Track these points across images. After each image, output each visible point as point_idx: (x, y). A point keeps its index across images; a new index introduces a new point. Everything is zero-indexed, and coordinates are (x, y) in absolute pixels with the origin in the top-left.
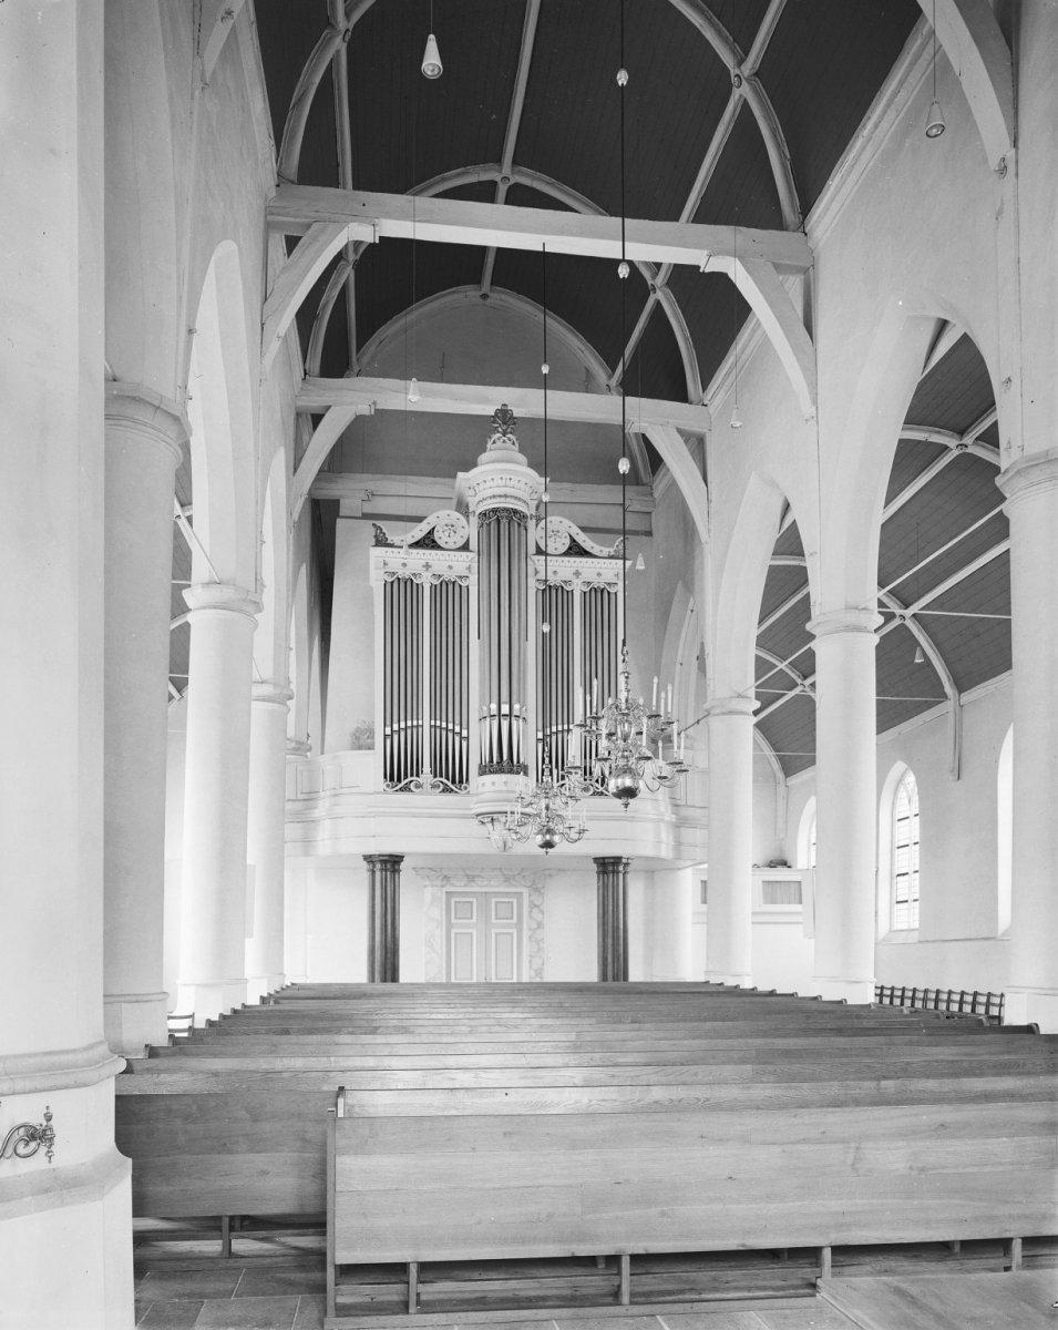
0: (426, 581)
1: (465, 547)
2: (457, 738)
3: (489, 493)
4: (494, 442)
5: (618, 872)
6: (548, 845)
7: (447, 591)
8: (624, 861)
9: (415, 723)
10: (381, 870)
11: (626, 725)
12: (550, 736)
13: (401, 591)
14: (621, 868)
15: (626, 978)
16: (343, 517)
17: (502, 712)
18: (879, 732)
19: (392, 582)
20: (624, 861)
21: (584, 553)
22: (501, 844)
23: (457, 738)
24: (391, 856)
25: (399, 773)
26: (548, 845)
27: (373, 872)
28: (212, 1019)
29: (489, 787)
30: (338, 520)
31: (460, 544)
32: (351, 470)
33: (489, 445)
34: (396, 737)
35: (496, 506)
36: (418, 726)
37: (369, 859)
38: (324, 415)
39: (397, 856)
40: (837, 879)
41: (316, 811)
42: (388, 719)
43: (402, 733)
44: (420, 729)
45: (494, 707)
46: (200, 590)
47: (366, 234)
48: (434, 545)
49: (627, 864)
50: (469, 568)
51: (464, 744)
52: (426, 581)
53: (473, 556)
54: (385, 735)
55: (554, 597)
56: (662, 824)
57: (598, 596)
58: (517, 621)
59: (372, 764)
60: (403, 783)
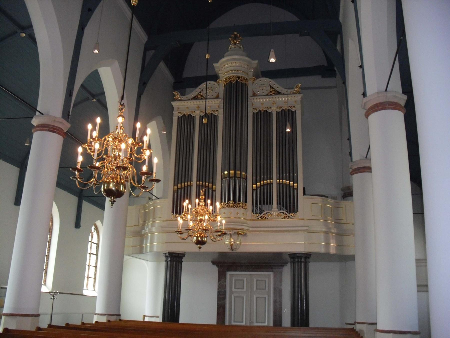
0: (274, 110)
1: (217, 97)
2: (210, 191)
5: (301, 262)
19: (257, 113)
21: (278, 93)
22: (229, 247)
28: (10, 328)
31: (215, 95)
33: (229, 49)
43: (183, 190)
50: (219, 106)
52: (197, 114)
55: (263, 117)
57: (287, 116)
58: (240, 130)
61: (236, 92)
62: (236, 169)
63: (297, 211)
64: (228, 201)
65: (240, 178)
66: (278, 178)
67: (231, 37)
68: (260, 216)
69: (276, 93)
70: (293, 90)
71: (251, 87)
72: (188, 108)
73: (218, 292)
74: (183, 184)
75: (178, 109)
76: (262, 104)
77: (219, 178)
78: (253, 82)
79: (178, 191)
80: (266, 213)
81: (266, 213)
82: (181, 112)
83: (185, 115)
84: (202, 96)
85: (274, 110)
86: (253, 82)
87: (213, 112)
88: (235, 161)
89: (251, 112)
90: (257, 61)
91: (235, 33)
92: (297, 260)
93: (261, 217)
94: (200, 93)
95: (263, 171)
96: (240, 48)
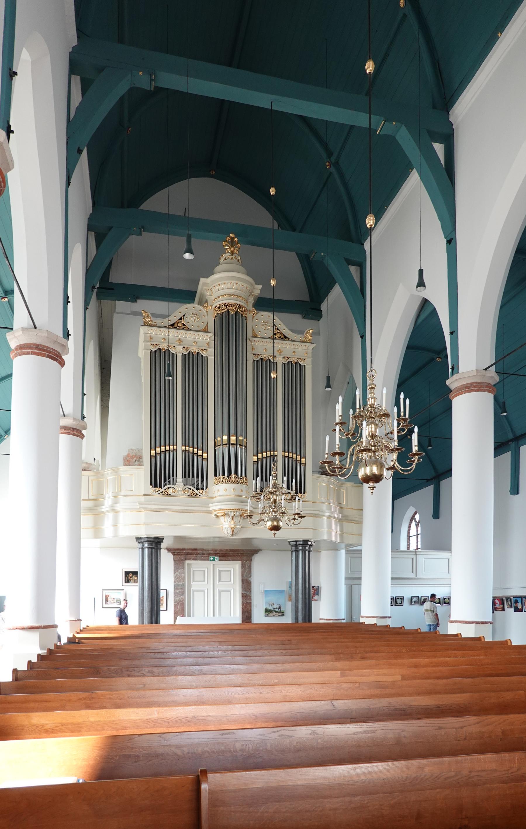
0: (179, 351)
1: (205, 330)
2: (200, 459)
3: (222, 292)
4: (225, 259)
6: (276, 528)
7: (194, 361)
8: (310, 543)
9: (167, 448)
10: (148, 548)
11: (373, 426)
12: (262, 459)
13: (161, 359)
14: (307, 548)
15: (310, 621)
16: (118, 313)
17: (232, 442)
18: (494, 457)
19: (155, 351)
20: (310, 543)
21: (285, 338)
22: (230, 531)
23: (200, 459)
24: (155, 538)
25: (160, 478)
26: (276, 528)
27: (143, 549)
29: (222, 492)
30: (114, 314)
31: (202, 327)
32: (3, 603)
33: (222, 260)
34: (158, 457)
35: (227, 301)
36: (173, 450)
37: (139, 540)
38: (107, 234)
39: (159, 538)
40: (379, 566)
41: (103, 507)
42: (153, 447)
44: (175, 453)
45: (225, 438)
46: (21, 333)
47: (142, 80)
48: (184, 328)
49: (311, 545)
51: (205, 463)
53: (211, 335)
54: (151, 456)
55: (264, 366)
56: (333, 520)
59: (142, 474)
60: (164, 488)
61: (229, 325)
62: (231, 434)
63: (207, 487)
64: (228, 477)
65: (236, 444)
66: (184, 444)
67: (226, 241)
68: (161, 490)
69: (283, 337)
70: (302, 336)
71: (250, 324)
72: (294, 352)
73: (175, 586)
74: (163, 448)
75: (151, 338)
76: (265, 349)
77: (211, 444)
78: (253, 317)
79: (156, 456)
80: (169, 488)
81: (169, 488)
82: (155, 343)
83: (160, 349)
84: (184, 325)
85: (179, 351)
86: (253, 317)
87: (200, 351)
88: (232, 424)
89: (251, 358)
90: (260, 287)
91: (232, 235)
92: (301, 548)
93: (162, 492)
94: (181, 319)
95: (265, 439)
96: (238, 261)
